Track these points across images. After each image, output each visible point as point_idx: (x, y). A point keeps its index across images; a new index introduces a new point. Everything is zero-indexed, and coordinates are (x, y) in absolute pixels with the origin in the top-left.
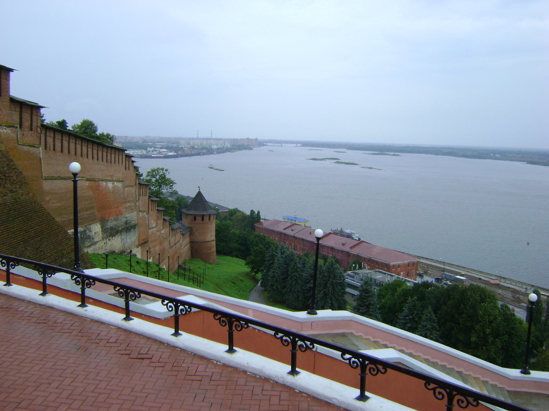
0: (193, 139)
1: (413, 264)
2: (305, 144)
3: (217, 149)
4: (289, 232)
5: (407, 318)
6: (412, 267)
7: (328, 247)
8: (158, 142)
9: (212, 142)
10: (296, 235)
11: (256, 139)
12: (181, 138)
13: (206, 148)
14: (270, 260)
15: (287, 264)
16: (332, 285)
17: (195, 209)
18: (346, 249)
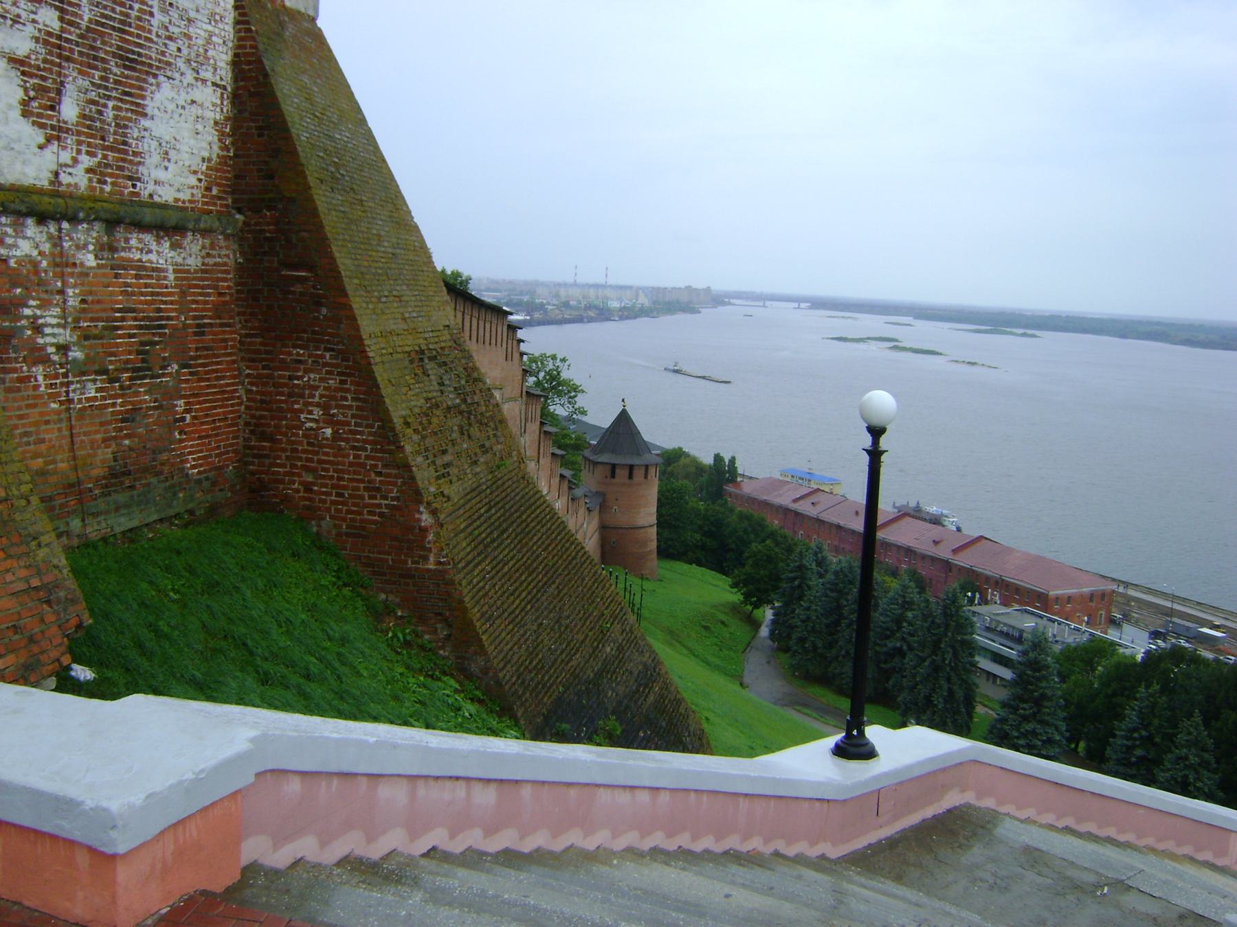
0: (566, 285)
1: (1103, 595)
2: (818, 304)
3: (621, 309)
4: (804, 507)
5: (1136, 735)
6: (1107, 603)
7: (899, 547)
8: (488, 290)
9: (609, 293)
10: (825, 517)
11: (708, 290)
12: (537, 284)
13: (596, 307)
14: (795, 578)
15: (840, 592)
16: (953, 647)
17: (614, 451)
18: (944, 552)
